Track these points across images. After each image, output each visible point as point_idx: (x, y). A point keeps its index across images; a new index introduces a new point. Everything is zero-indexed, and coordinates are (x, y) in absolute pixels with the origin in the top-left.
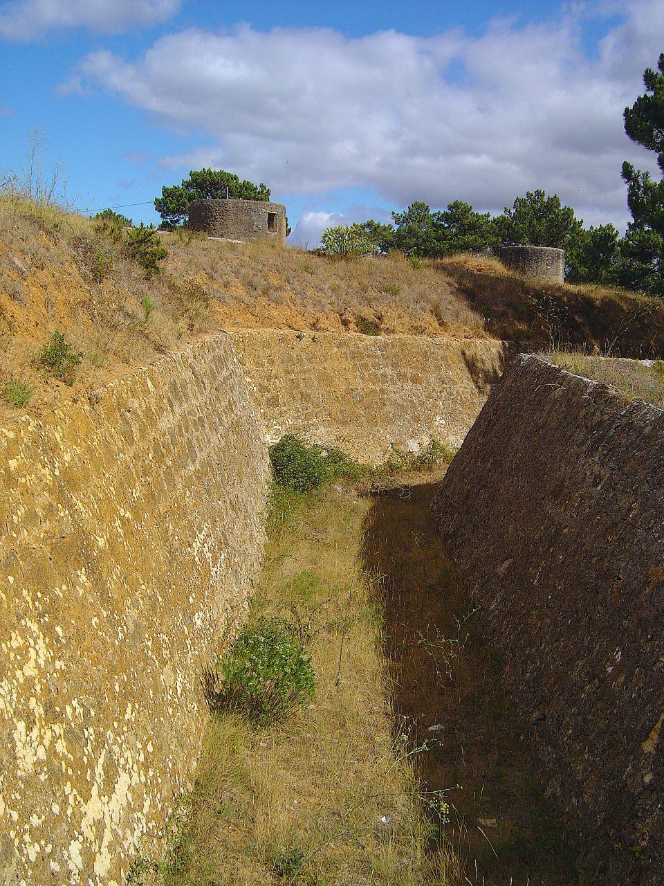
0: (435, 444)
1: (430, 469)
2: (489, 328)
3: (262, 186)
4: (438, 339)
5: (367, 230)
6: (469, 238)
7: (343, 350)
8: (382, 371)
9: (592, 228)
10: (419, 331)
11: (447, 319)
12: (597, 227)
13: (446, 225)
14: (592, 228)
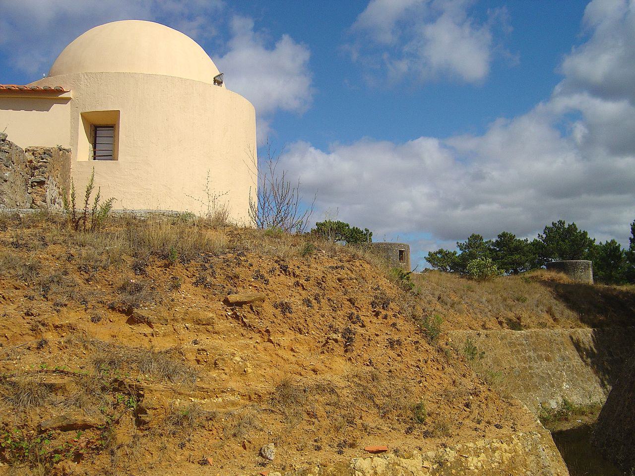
0: (565, 402)
1: (566, 419)
2: (582, 320)
3: (366, 230)
4: (556, 330)
5: (439, 256)
6: (516, 257)
7: (504, 341)
8: (528, 354)
9: (601, 243)
10: (543, 325)
11: (558, 316)
12: (604, 243)
13: (498, 249)
14: (601, 243)
